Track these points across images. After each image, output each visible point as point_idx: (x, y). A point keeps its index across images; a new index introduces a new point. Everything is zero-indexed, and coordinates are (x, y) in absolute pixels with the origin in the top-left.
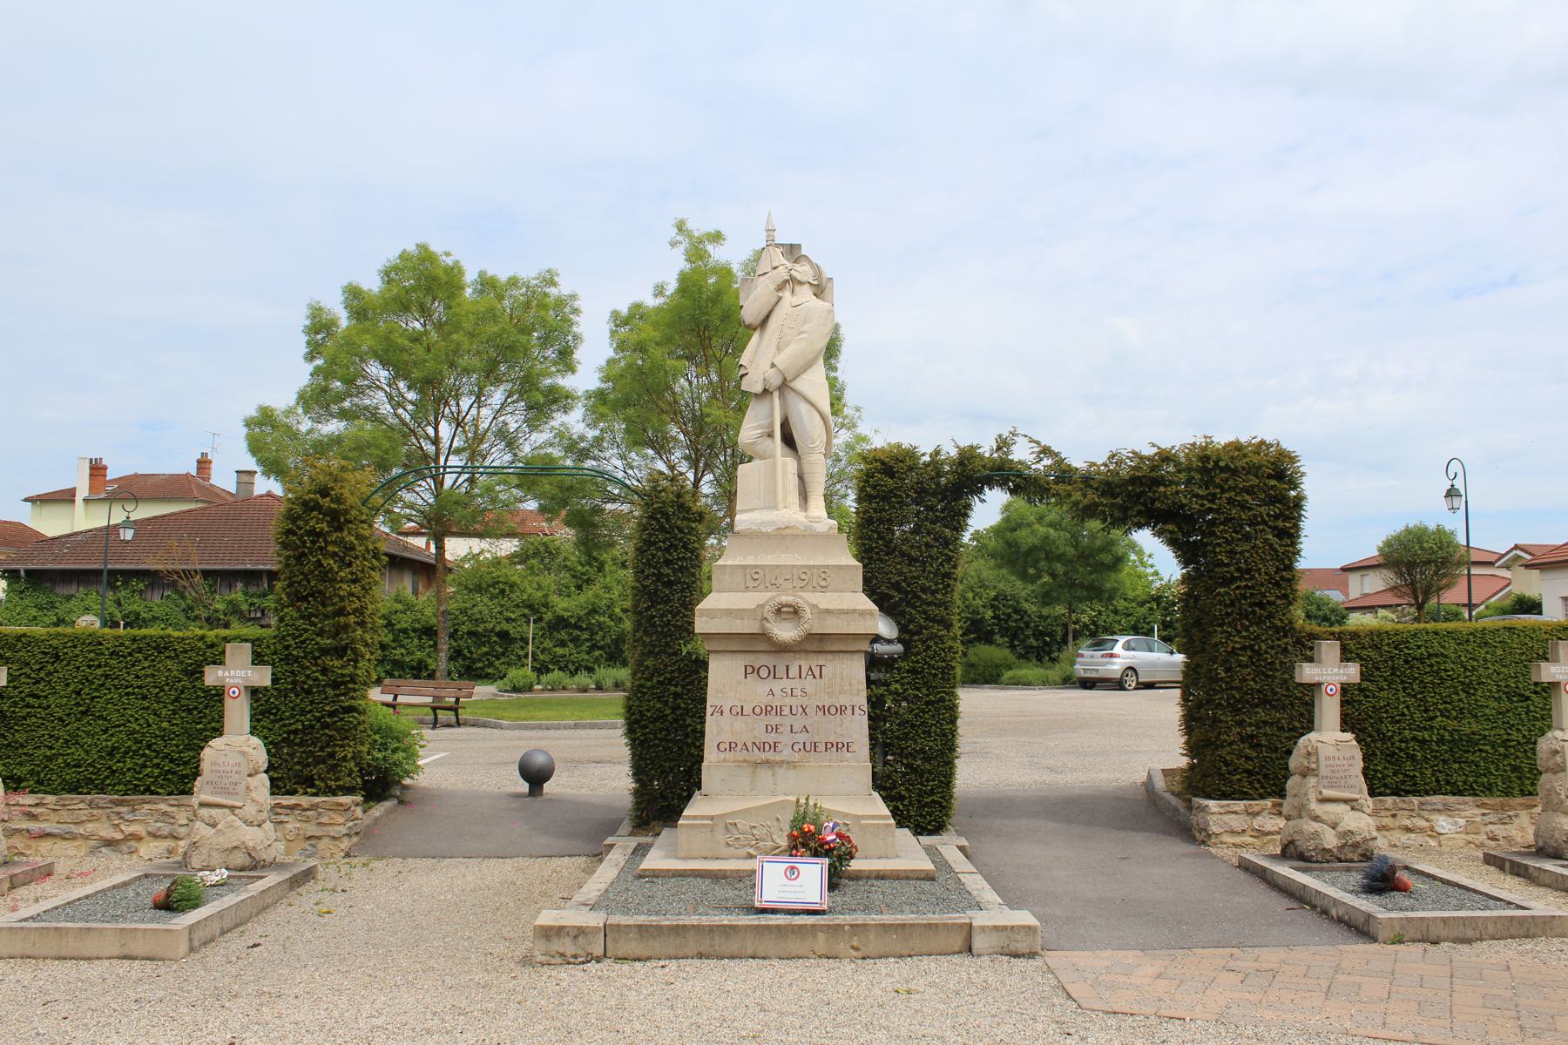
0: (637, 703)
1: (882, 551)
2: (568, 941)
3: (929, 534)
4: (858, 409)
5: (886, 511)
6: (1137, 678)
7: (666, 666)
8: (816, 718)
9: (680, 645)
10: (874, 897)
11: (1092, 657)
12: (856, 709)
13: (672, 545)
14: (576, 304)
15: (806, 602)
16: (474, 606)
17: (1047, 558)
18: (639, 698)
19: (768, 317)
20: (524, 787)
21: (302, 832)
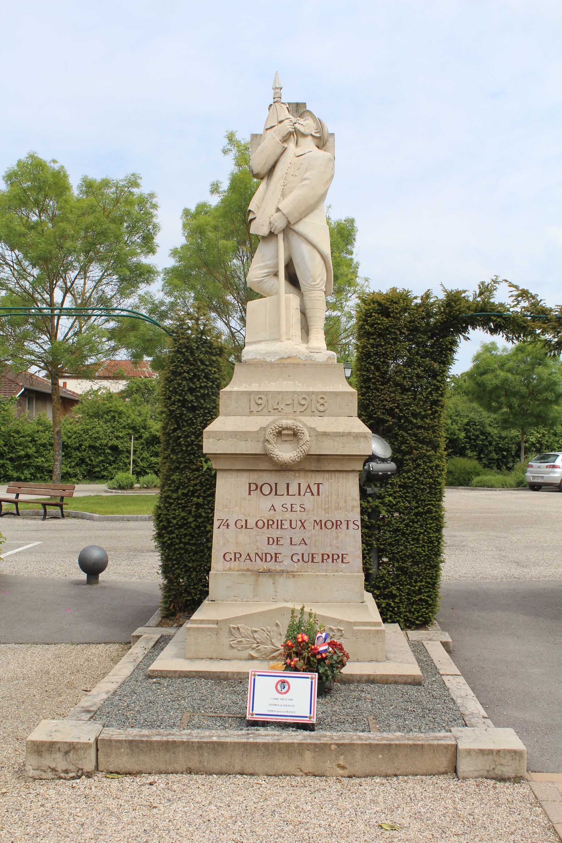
1: (378, 381)
3: (419, 366)
4: (367, 280)
5: (381, 346)
8: (314, 532)
9: (201, 462)
10: (365, 705)
11: (539, 467)
12: (351, 525)
13: (195, 376)
14: (154, 201)
15: (305, 425)
17: (506, 395)
18: (166, 508)
19: (274, 167)
20: (84, 576)
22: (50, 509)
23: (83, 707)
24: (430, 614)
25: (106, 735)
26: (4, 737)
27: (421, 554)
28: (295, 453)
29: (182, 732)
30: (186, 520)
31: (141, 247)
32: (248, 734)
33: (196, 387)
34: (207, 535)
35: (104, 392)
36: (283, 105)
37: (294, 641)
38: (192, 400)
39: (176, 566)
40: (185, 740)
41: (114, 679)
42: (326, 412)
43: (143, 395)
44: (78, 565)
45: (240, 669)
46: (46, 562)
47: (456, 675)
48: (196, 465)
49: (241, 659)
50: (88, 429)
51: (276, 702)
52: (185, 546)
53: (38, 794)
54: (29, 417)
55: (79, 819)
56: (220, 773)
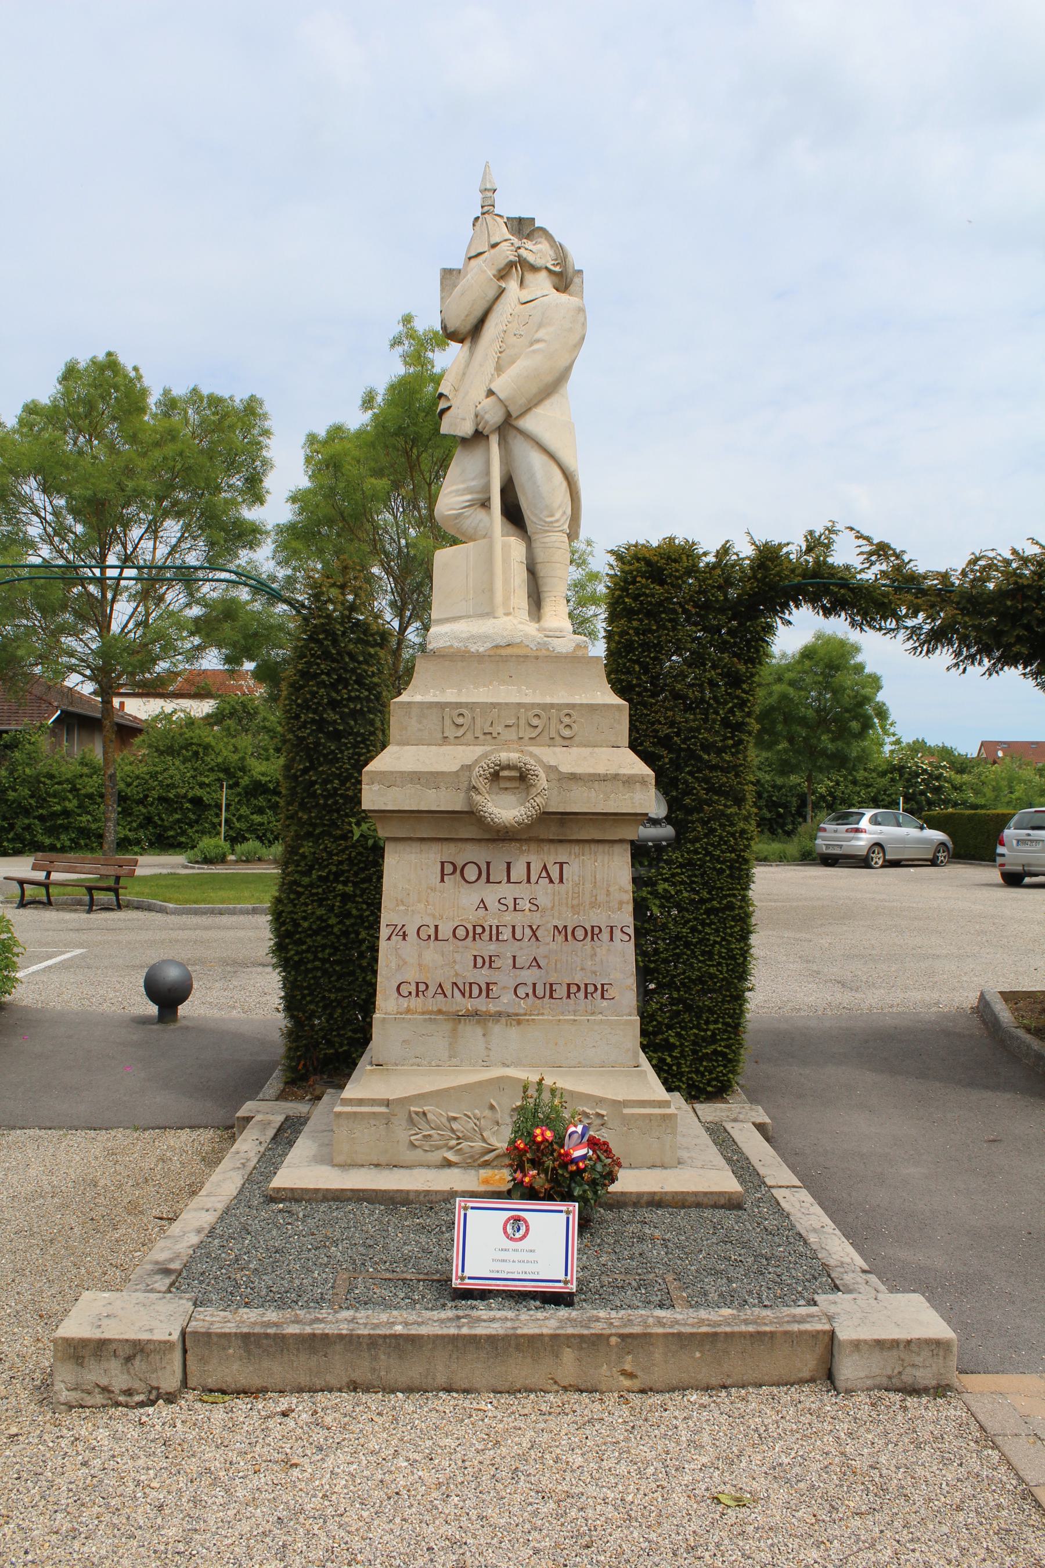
0: (290, 908)
2: (114, 1365)
5: (651, 631)
6: (884, 855)
7: (331, 854)
8: (553, 946)
9: (350, 823)
11: (836, 831)
12: (617, 933)
13: (340, 680)
15: (540, 761)
16: (165, 770)
18: (292, 901)
20: (153, 1010)
22: (98, 896)
23: (157, 1263)
24: (731, 1076)
25: (201, 1324)
26: (18, 1312)
27: (716, 977)
28: (523, 810)
29: (337, 1315)
30: (325, 921)
31: (241, 492)
32: (459, 1318)
33: (342, 698)
34: (359, 947)
35: (182, 716)
36: (498, 218)
37: (528, 1139)
38: (335, 721)
39: (308, 999)
40: (344, 1332)
41: (210, 1202)
42: (575, 738)
43: (240, 721)
44: (143, 989)
45: (429, 1184)
46: (92, 984)
47: (794, 1187)
48: (342, 829)
49: (429, 1166)
50: (157, 773)
52: (323, 964)
53: (77, 1439)
54: (69, 755)
55: (154, 1494)
56: (409, 1390)
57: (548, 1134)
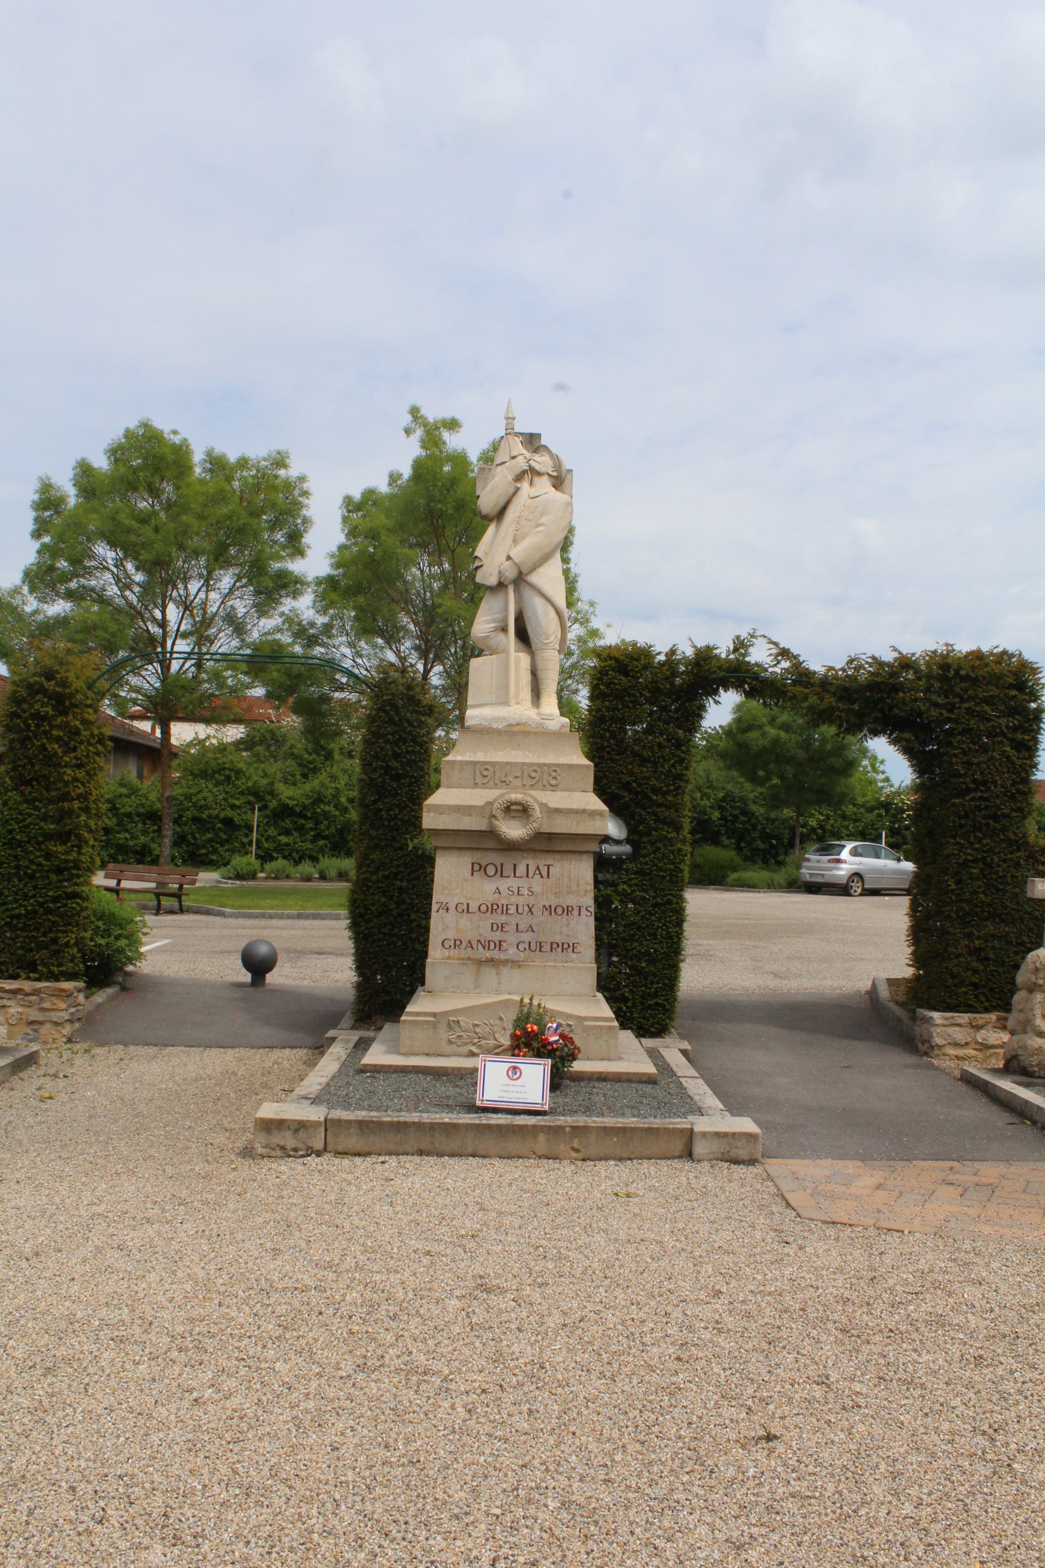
2: (288, 1134)
4: (592, 604)
5: (618, 709)
6: (863, 884)
7: (392, 860)
8: (542, 918)
9: (406, 839)
11: (818, 861)
12: (584, 911)
13: (400, 739)
14: (305, 486)
15: (536, 800)
16: (198, 792)
20: (246, 977)
21: (24, 1017)
43: (268, 748)
49: (460, 1056)
50: (191, 794)
51: (507, 1088)
56: (452, 1155)
57: (535, 1027)
